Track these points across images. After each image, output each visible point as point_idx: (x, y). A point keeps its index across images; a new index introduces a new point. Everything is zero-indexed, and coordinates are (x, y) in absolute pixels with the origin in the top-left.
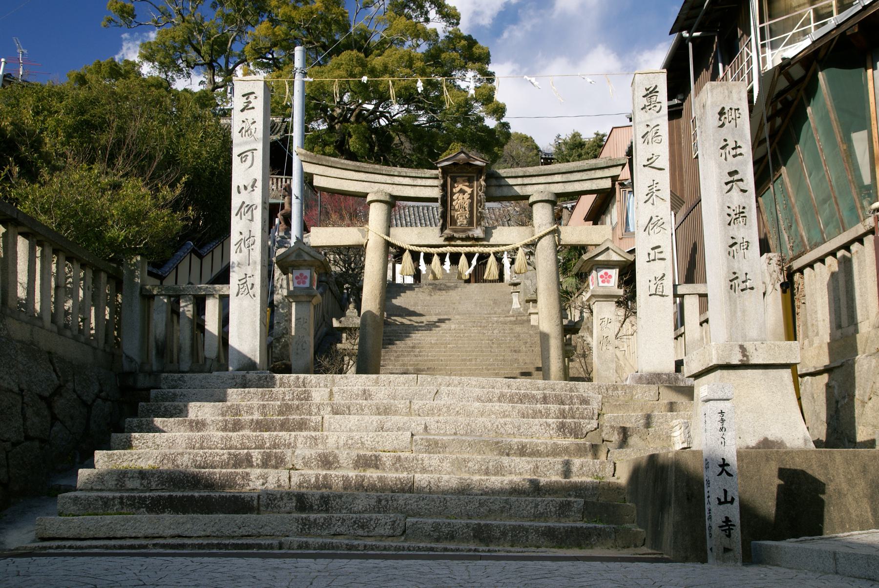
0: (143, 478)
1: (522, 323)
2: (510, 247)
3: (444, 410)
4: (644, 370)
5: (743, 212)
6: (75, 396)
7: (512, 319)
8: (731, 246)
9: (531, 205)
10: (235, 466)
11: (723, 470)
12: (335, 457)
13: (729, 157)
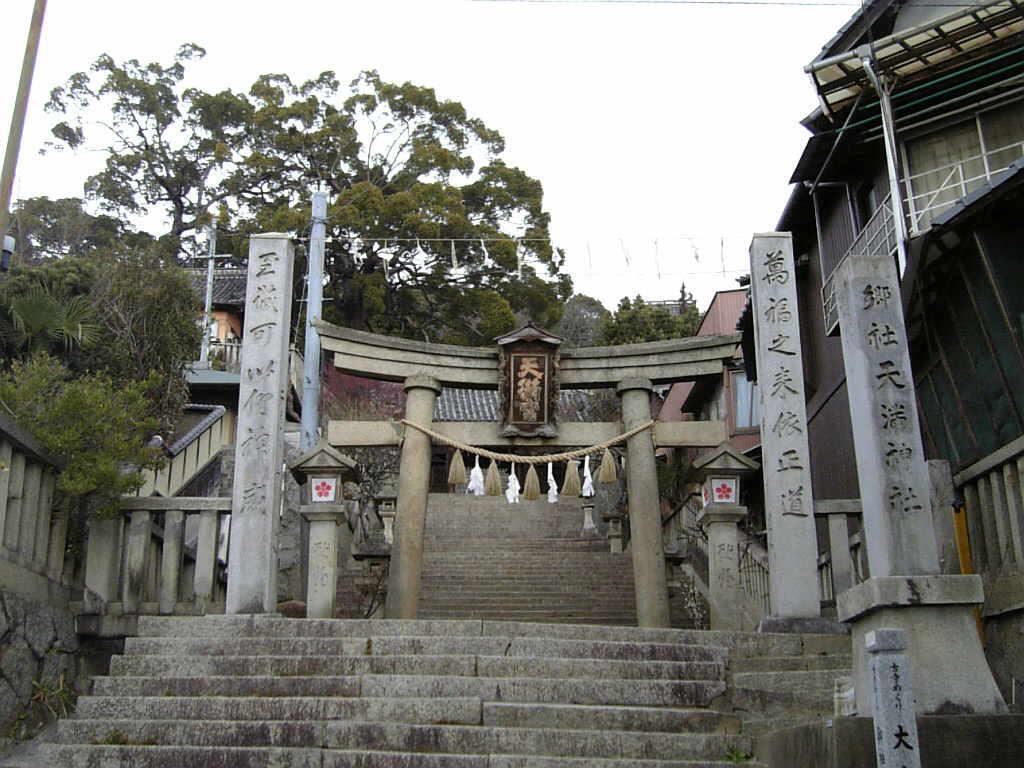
0: (124, 759)
1: (597, 549)
2: (590, 449)
3: (521, 668)
4: (780, 613)
5: (901, 413)
6: (26, 646)
7: (583, 543)
8: (889, 454)
9: (620, 394)
10: (245, 743)
11: (901, 741)
12: (382, 732)
13: (881, 346)
